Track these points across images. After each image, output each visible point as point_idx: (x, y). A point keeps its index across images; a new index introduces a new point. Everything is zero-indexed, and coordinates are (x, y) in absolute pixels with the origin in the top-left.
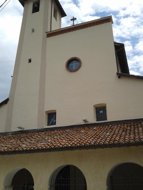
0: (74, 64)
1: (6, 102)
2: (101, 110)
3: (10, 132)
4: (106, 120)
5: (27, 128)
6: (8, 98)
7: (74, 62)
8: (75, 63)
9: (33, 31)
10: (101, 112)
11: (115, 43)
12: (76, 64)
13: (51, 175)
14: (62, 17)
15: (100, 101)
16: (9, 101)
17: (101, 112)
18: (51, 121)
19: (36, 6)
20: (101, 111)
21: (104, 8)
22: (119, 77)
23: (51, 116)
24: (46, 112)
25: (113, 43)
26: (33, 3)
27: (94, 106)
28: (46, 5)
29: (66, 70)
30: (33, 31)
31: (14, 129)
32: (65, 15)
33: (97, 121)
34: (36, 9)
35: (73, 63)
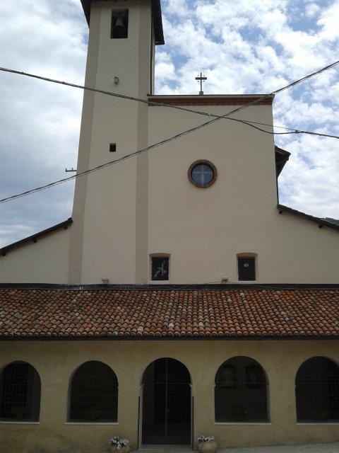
0: (203, 175)
1: (70, 221)
2: (246, 263)
3: (82, 286)
4: (254, 279)
5: (114, 280)
6: (70, 219)
7: (202, 167)
8: (206, 170)
9: (116, 83)
10: (246, 265)
11: (276, 148)
12: (206, 173)
13: (68, 412)
14: (157, 44)
15: (247, 249)
16: (73, 225)
17: (246, 265)
18: (158, 272)
19: (119, 23)
20: (247, 265)
21: (296, 126)
22: (280, 213)
23: (160, 264)
24: (150, 255)
25: (274, 148)
26: (113, 13)
27: (237, 255)
28: (138, 21)
29: (189, 183)
30: (116, 83)
31: (92, 277)
32: (162, 43)
33: (240, 280)
34: (119, 31)
35: (200, 170)
